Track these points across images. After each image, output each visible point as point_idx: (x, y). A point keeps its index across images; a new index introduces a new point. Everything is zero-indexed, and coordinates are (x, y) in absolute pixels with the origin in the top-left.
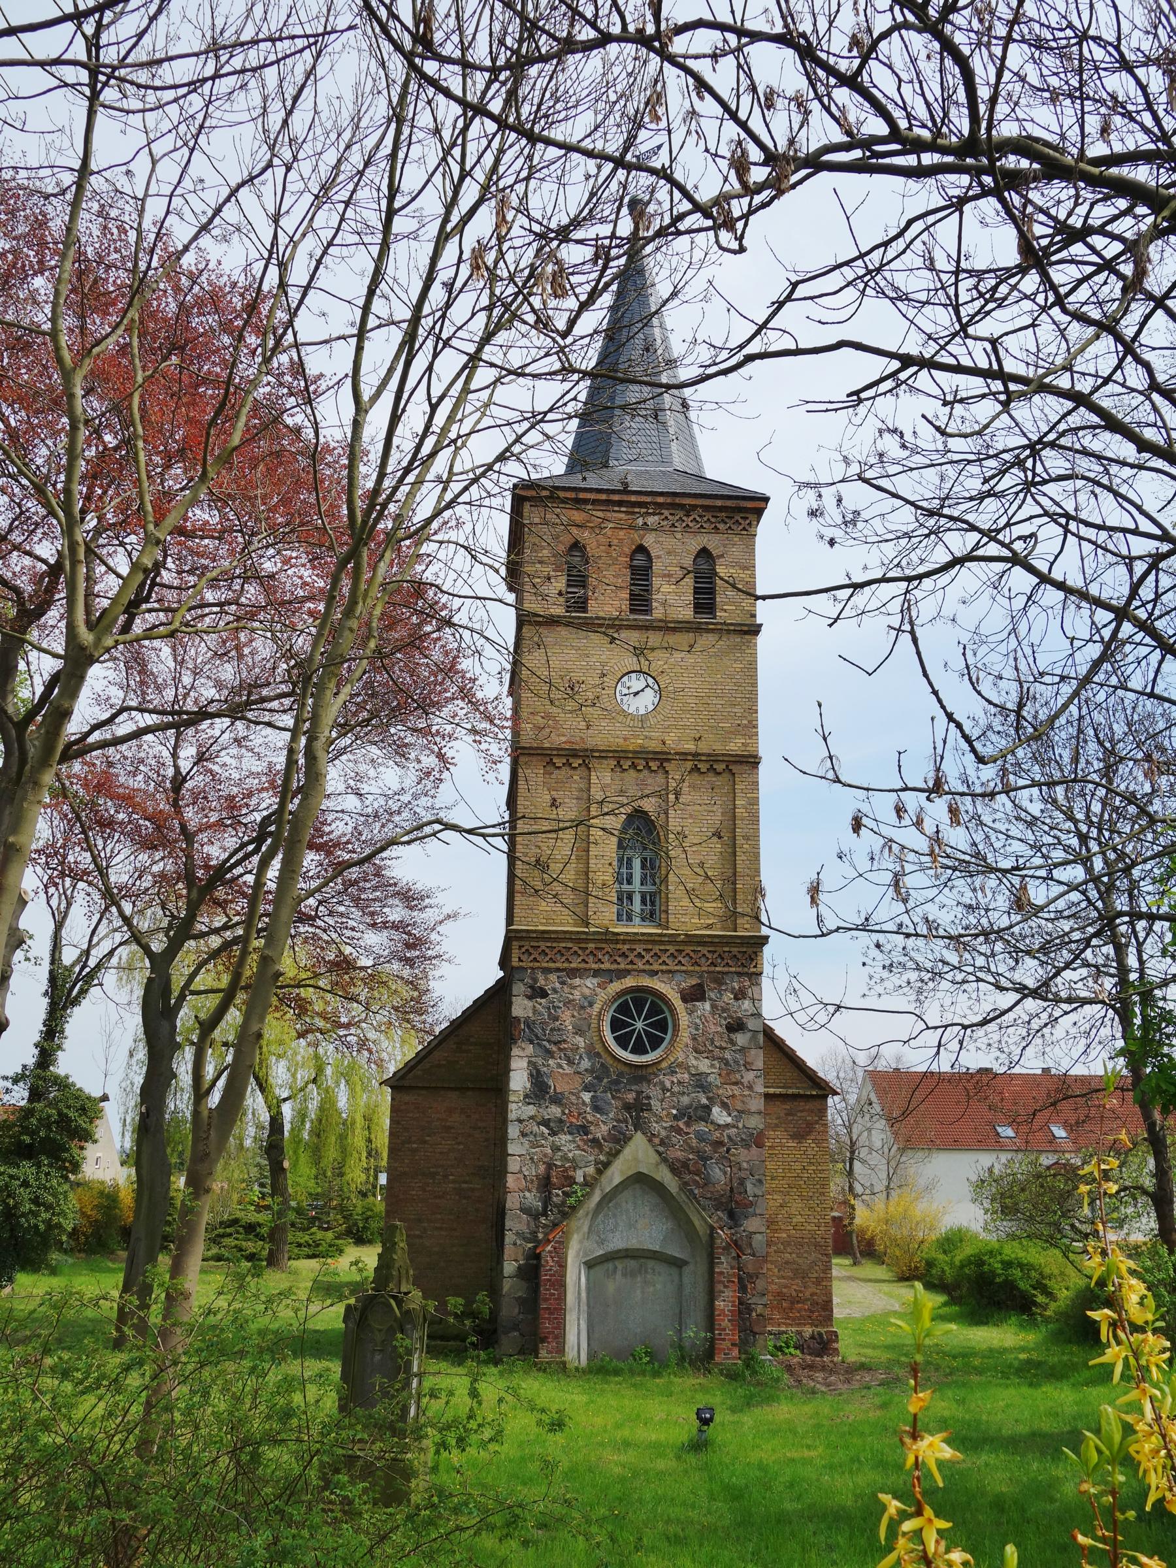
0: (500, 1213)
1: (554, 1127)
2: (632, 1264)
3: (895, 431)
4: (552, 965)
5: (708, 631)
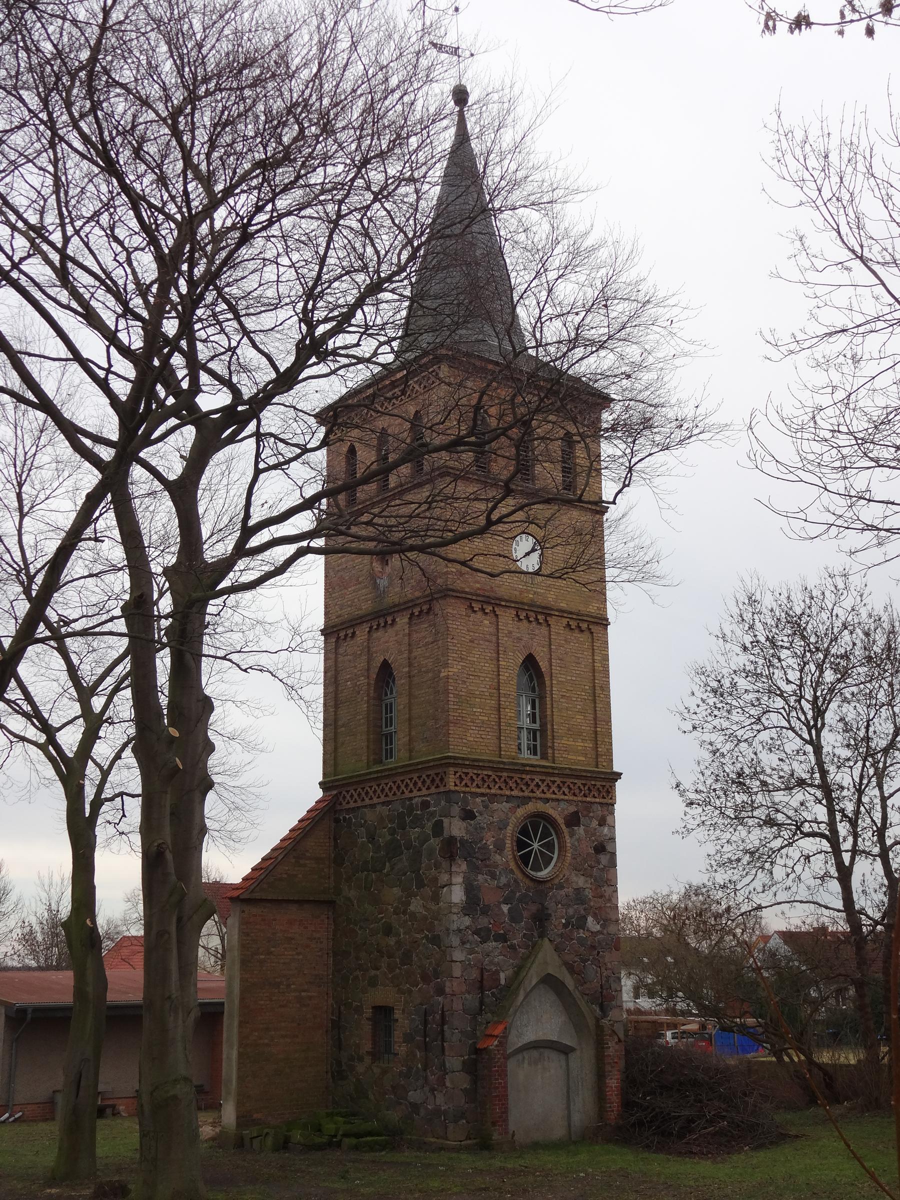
1: (484, 935)
2: (535, 1053)
4: (478, 790)
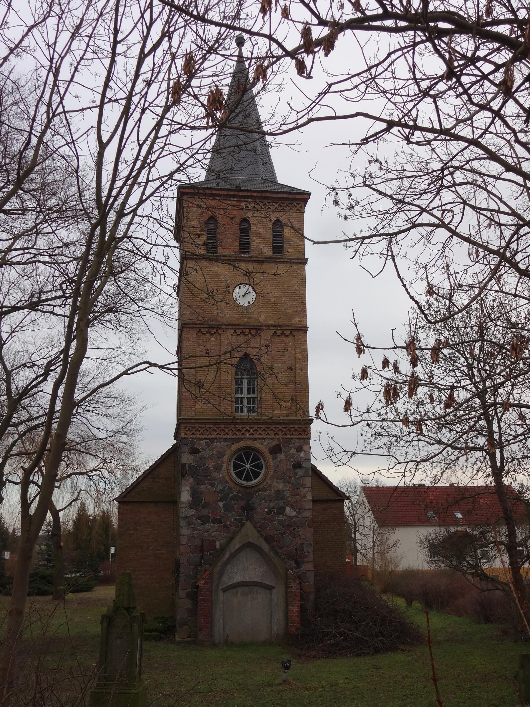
0: (177, 565)
2: (247, 589)
3: (377, 161)
5: (283, 262)
